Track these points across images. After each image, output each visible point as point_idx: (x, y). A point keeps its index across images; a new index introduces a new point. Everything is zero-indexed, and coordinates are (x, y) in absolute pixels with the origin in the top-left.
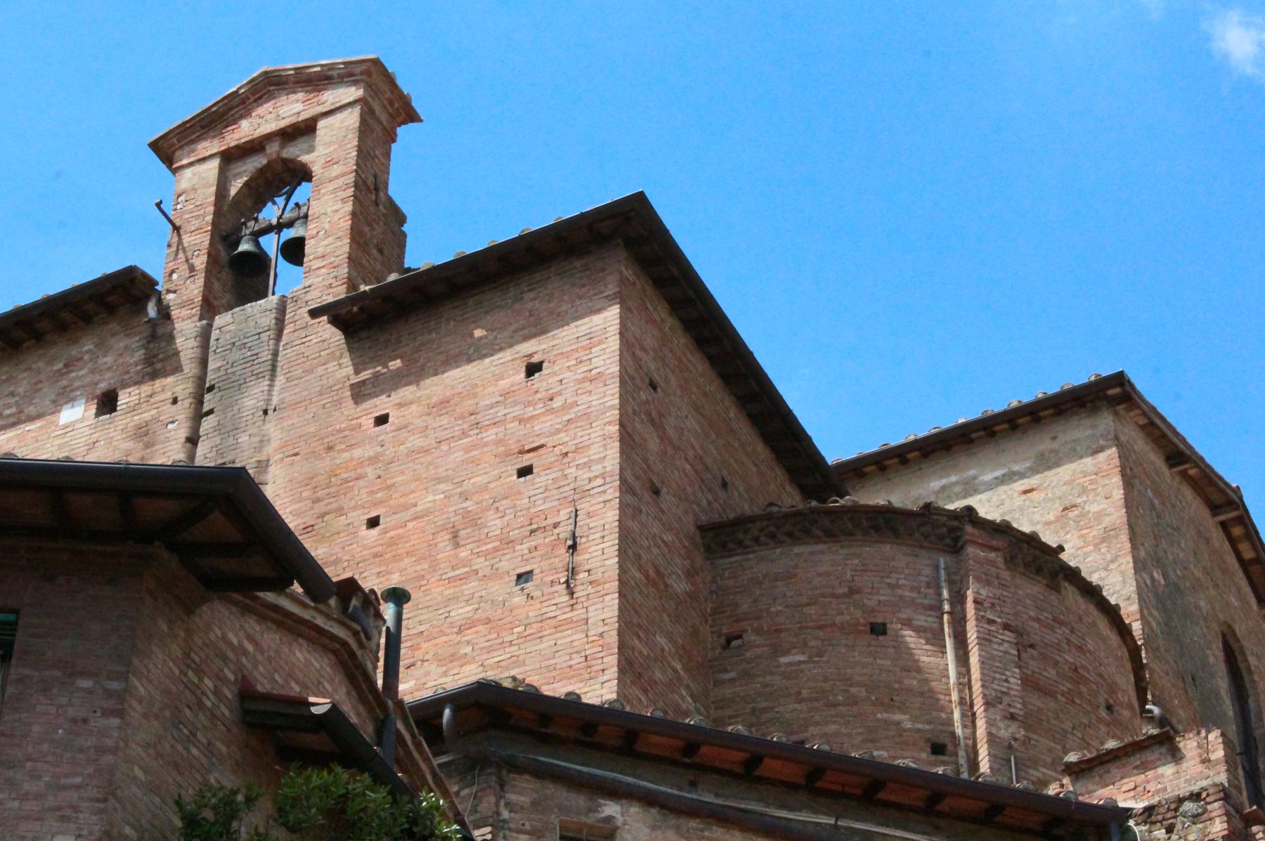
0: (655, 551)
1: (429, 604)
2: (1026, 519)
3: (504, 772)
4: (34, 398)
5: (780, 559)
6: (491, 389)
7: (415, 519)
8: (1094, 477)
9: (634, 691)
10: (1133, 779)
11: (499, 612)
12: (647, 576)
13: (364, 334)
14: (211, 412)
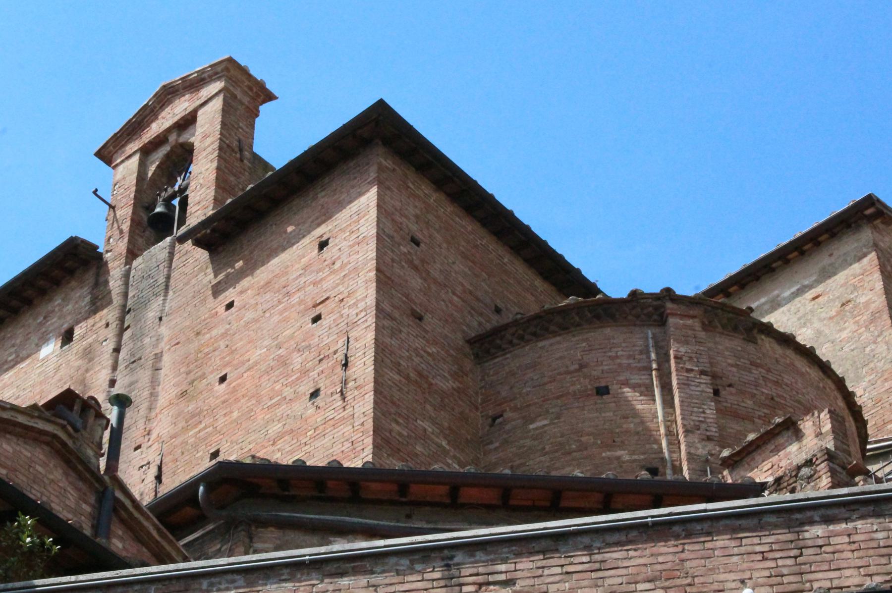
0: (417, 360)
1: (254, 428)
2: (816, 318)
3: (253, 528)
4: (26, 345)
5: (527, 354)
6: (297, 266)
7: (248, 370)
8: (861, 277)
9: (391, 461)
10: (770, 460)
11: (298, 423)
12: (407, 378)
13: (220, 249)
14: (128, 327)
